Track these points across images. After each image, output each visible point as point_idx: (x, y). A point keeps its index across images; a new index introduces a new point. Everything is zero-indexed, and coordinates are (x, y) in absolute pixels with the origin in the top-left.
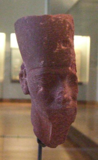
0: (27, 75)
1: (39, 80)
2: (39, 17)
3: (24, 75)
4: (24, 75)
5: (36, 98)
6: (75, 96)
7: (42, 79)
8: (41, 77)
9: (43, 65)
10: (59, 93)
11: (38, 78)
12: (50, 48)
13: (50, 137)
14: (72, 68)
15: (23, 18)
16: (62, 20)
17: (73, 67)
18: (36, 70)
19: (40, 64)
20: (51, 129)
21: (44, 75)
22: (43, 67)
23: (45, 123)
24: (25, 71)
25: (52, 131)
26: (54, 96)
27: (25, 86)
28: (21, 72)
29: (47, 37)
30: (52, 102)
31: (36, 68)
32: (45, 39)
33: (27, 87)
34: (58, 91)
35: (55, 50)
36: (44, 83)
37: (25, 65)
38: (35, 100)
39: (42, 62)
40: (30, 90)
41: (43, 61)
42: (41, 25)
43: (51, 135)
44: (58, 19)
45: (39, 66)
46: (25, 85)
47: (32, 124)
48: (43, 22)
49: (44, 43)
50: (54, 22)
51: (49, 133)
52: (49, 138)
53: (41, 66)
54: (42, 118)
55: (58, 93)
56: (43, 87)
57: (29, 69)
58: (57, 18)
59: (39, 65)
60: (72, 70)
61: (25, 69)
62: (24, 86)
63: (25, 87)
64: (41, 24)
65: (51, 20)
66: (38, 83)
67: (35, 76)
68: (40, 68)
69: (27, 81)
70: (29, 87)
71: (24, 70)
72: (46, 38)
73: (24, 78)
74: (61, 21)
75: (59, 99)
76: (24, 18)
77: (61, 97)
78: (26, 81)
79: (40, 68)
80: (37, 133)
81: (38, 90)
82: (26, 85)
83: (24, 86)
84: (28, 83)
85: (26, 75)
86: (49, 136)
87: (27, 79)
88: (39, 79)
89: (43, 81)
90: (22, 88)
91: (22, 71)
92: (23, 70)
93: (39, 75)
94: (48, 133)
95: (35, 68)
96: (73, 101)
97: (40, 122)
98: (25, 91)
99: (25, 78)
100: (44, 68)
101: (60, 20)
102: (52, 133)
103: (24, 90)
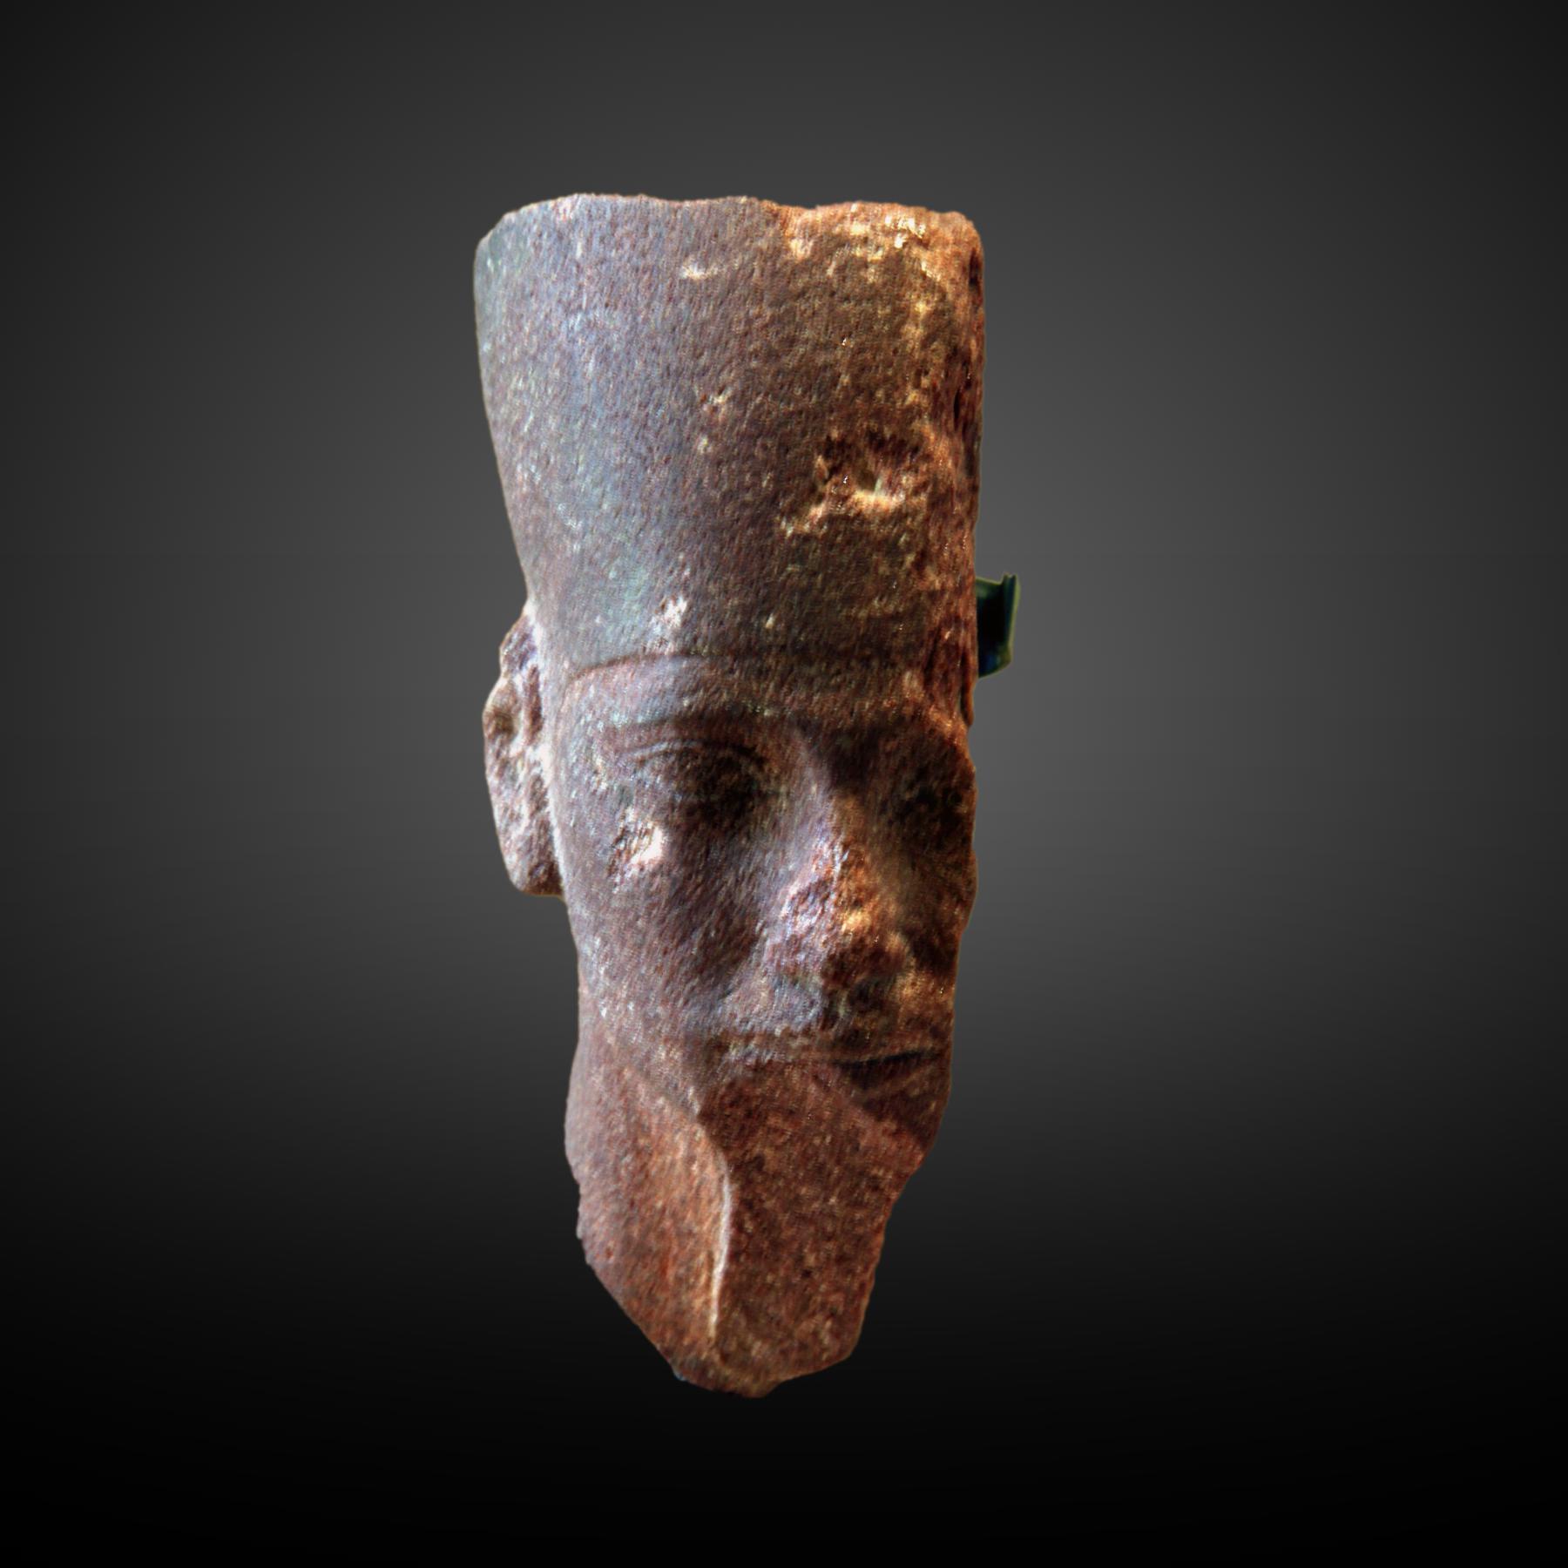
0: (548, 725)
1: (642, 762)
3: (522, 721)
4: (522, 721)
5: (603, 923)
6: (940, 932)
7: (666, 754)
8: (659, 740)
9: (677, 636)
10: (803, 896)
12: (748, 497)
13: (715, 1291)
14: (927, 682)
16: (879, 255)
17: (937, 671)
18: (621, 675)
19: (657, 630)
20: (725, 1220)
21: (684, 722)
22: (674, 656)
24: (533, 689)
25: (734, 1242)
26: (755, 917)
27: (525, 822)
29: (729, 392)
30: (735, 962)
31: (625, 659)
32: (715, 409)
33: (545, 827)
34: (791, 877)
35: (795, 511)
36: (727, 1063)
38: (598, 942)
39: (676, 610)
41: (683, 605)
42: (690, 281)
43: (727, 1275)
44: (843, 241)
45: (651, 644)
46: (525, 809)
48: (705, 263)
49: (703, 443)
50: (806, 266)
51: (711, 1263)
52: (707, 1303)
53: (663, 642)
54: (655, 1120)
55: (793, 890)
56: (667, 824)
57: (505, 700)
58: (837, 230)
59: (645, 633)
60: (932, 698)
61: (535, 672)
64: (693, 272)
65: (779, 250)
66: (624, 797)
67: (611, 733)
68: (653, 658)
69: (548, 779)
71: (525, 672)
72: (720, 400)
74: (865, 264)
75: (795, 944)
77: (810, 929)
78: (538, 779)
79: (653, 658)
81: (620, 853)
82: (532, 815)
84: (551, 798)
85: (536, 717)
86: (708, 1286)
87: (543, 753)
88: (638, 755)
89: (669, 777)
93: (640, 720)
94: (702, 1257)
95: (612, 663)
97: (638, 1152)
99: (529, 750)
100: (685, 664)
101: (858, 252)
102: (733, 1256)
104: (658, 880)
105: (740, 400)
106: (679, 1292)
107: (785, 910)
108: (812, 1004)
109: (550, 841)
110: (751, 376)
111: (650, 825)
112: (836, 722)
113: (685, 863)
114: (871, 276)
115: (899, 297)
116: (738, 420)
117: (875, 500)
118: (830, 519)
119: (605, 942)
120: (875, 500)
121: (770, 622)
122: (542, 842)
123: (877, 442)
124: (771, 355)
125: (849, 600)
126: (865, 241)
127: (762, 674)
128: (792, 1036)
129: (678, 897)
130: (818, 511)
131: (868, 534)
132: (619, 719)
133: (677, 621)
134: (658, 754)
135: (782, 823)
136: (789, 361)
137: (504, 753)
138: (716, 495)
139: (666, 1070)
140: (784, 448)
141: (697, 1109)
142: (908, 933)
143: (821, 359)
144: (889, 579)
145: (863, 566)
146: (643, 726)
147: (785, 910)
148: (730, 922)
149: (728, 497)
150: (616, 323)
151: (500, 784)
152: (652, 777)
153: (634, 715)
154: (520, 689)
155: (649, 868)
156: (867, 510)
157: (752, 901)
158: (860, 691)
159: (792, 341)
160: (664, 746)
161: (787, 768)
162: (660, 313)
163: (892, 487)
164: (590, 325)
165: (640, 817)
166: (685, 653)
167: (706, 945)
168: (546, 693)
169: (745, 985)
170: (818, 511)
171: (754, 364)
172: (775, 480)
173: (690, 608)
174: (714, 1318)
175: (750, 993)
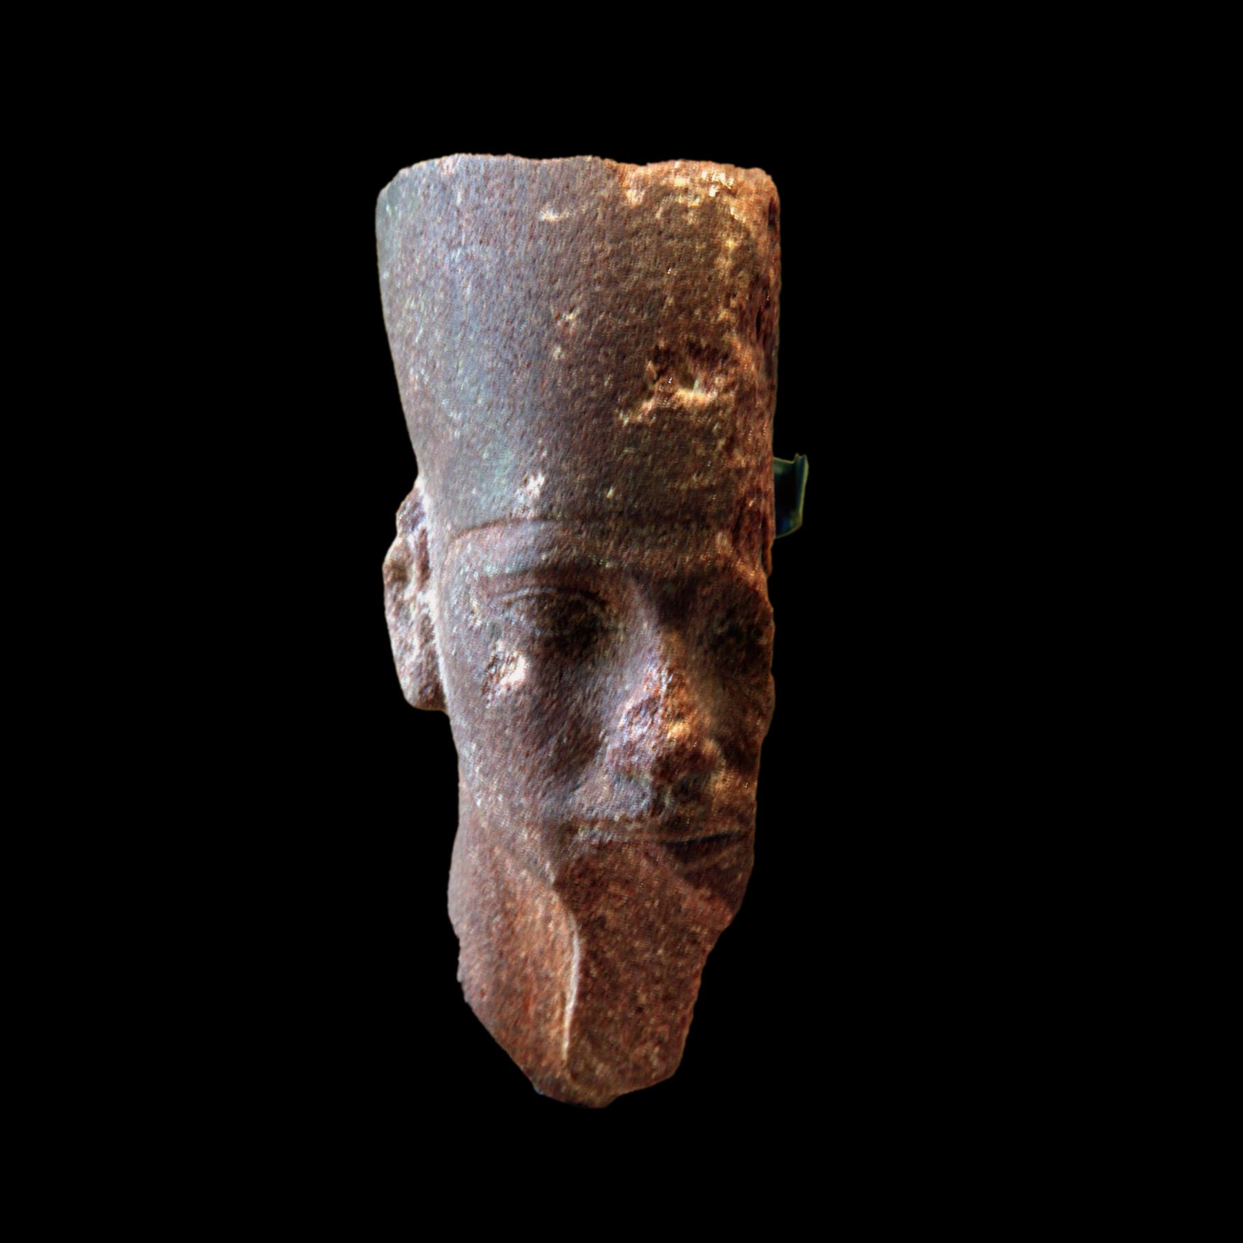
0: (434, 575)
1: (509, 604)
3: (414, 571)
4: (414, 571)
5: (478, 732)
6: (745, 739)
7: (528, 598)
8: (523, 587)
9: (537, 504)
10: (637, 710)
11: (501, 594)
12: (593, 394)
13: (567, 1024)
14: (735, 541)
16: (697, 202)
17: (743, 532)
18: (492, 535)
19: (521, 499)
20: (575, 967)
21: (542, 572)
22: (534, 520)
23: (538, 926)
24: (423, 546)
25: (582, 984)
26: (599, 727)
27: (416, 651)
29: (578, 311)
30: (583, 763)
31: (495, 523)
32: (567, 324)
33: (432, 655)
34: (627, 695)
35: (630, 405)
36: (577, 843)
38: (474, 747)
39: (536, 484)
41: (541, 480)
42: (547, 223)
43: (577, 1010)
44: (668, 191)
45: (516, 510)
48: (559, 209)
49: (557, 351)
50: (639, 211)
51: (563, 1001)
52: (561, 1033)
53: (525, 509)
54: (519, 888)
55: (629, 705)
56: (529, 654)
58: (663, 182)
59: (511, 502)
60: (739, 553)
61: (424, 532)
64: (549, 216)
66: (495, 632)
67: (484, 581)
68: (517, 521)
69: (434, 617)
71: (417, 533)
72: (571, 317)
74: (686, 210)
75: (630, 748)
77: (642, 736)
78: (427, 618)
79: (517, 521)
81: (491, 677)
82: (422, 646)
84: (437, 632)
85: (425, 569)
86: (561, 1019)
87: (431, 597)
88: (506, 598)
89: (530, 616)
93: (507, 570)
94: (557, 997)
95: (485, 525)
97: (506, 913)
99: (420, 595)
100: (543, 526)
101: (680, 200)
102: (581, 996)
104: (521, 697)
105: (586, 317)
107: (623, 722)
108: (644, 796)
109: (436, 667)
110: (595, 298)
111: (515, 654)
113: (543, 684)
114: (691, 219)
116: (585, 333)
117: (694, 396)
118: (658, 411)
119: (480, 747)
120: (694, 396)
121: (611, 493)
122: (430, 667)
123: (695, 350)
124: (611, 282)
125: (673, 476)
126: (686, 191)
127: (604, 534)
128: (628, 821)
129: (537, 711)
130: (649, 405)
131: (688, 423)
132: (490, 570)
133: (537, 492)
134: (521, 598)
135: (620, 652)
136: (626, 287)
137: (400, 597)
138: (568, 392)
139: (528, 848)
140: (622, 355)
141: (552, 879)
142: (720, 740)
143: (651, 284)
144: (705, 459)
145: (684, 449)
146: (510, 575)
147: (623, 722)
148: (578, 731)
149: (577, 394)
152: (517, 616)
153: (502, 567)
154: (412, 546)
155: (514, 688)
156: (687, 404)
157: (596, 714)
158: (681, 548)
159: (627, 271)
160: (526, 592)
161: (624, 609)
163: (707, 386)
164: (468, 258)
165: (507, 648)
166: (543, 517)
167: (560, 749)
168: (433, 549)
169: (591, 781)
170: (649, 405)
171: (598, 288)
172: (615, 381)
173: (547, 482)
174: (566, 1045)
175: (595, 787)
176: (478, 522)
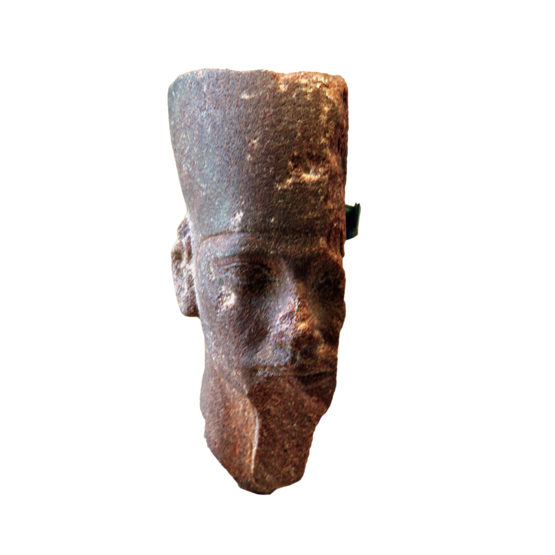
0: (194, 257)
1: (227, 270)
2: (238, 74)
3: (185, 255)
4: (185, 255)
5: (213, 327)
6: (333, 330)
7: (236, 267)
8: (233, 262)
9: (240, 225)
10: (284, 317)
11: (224, 265)
12: (265, 176)
13: (253, 457)
14: (328, 241)
15: (192, 73)
16: (311, 90)
17: (332, 238)
18: (220, 239)
19: (233, 223)
20: (257, 432)
21: (242, 256)
22: (239, 232)
24: (189, 244)
25: (260, 440)
26: (267, 324)
27: (186, 291)
28: (177, 245)
29: (258, 139)
30: (260, 341)
31: (221, 233)
32: (253, 145)
33: (193, 293)
34: (280, 310)
35: (281, 181)
37: (191, 225)
38: (212, 333)
39: (239, 216)
40: (198, 302)
41: (242, 214)
42: (244, 100)
43: (257, 451)
44: (298, 85)
45: (230, 228)
46: (186, 286)
47: (203, 414)
48: (249, 93)
49: (249, 157)
50: (285, 94)
51: (252, 447)
52: (250, 461)
53: (235, 227)
55: (281, 315)
56: (236, 292)
57: (179, 248)
60: (330, 247)
61: (189, 238)
62: (182, 289)
63: (184, 294)
64: (245, 96)
65: (276, 88)
66: (221, 282)
67: (216, 260)
68: (231, 233)
69: (194, 276)
70: (197, 295)
72: (255, 141)
73: (184, 262)
74: (306, 94)
75: (281, 334)
76: (194, 74)
78: (191, 276)
79: (231, 233)
80: (216, 444)
82: (188, 289)
83: (182, 289)
84: (195, 282)
85: (190, 254)
86: (251, 455)
87: (192, 267)
88: (226, 267)
89: (237, 275)
90: (178, 295)
91: (181, 244)
92: (184, 241)
93: (227, 255)
94: (249, 445)
95: (217, 235)
96: (325, 343)
97: (226, 408)
98: (185, 307)
99: (187, 266)
100: (242, 235)
101: (304, 89)
102: (260, 445)
103: (182, 303)
104: (233, 311)
105: (262, 142)
106: (240, 457)
107: (278, 322)
108: (287, 355)
110: (266, 133)
111: (230, 292)
112: (296, 256)
113: (242, 305)
114: (308, 98)
115: (318, 105)
116: (261, 149)
117: (310, 177)
118: (294, 184)
119: (214, 333)
120: (310, 177)
121: (273, 220)
123: (310, 156)
124: (273, 126)
125: (300, 212)
126: (306, 85)
127: (270, 238)
128: (280, 367)
129: (240, 318)
130: (290, 181)
131: (307, 189)
132: (219, 254)
133: (240, 220)
134: (233, 267)
135: (277, 291)
137: (178, 267)
138: (254, 175)
139: (236, 379)
140: (278, 158)
141: (247, 392)
142: (322, 330)
143: (291, 127)
144: (315, 205)
145: (305, 200)
146: (228, 257)
147: (278, 322)
148: (258, 326)
149: (258, 176)
150: (218, 114)
151: (177, 277)
152: (231, 275)
153: (224, 253)
154: (184, 244)
155: (230, 307)
156: (307, 180)
157: (266, 319)
158: (304, 244)
159: (280, 121)
160: (235, 264)
161: (279, 272)
162: (234, 111)
163: (316, 172)
164: (209, 115)
165: (227, 289)
166: (242, 231)
167: (250, 335)
168: (193, 245)
170: (290, 181)
171: (267, 129)
172: (274, 170)
173: (244, 215)
174: (253, 467)
175: (266, 352)
176: (214, 233)
